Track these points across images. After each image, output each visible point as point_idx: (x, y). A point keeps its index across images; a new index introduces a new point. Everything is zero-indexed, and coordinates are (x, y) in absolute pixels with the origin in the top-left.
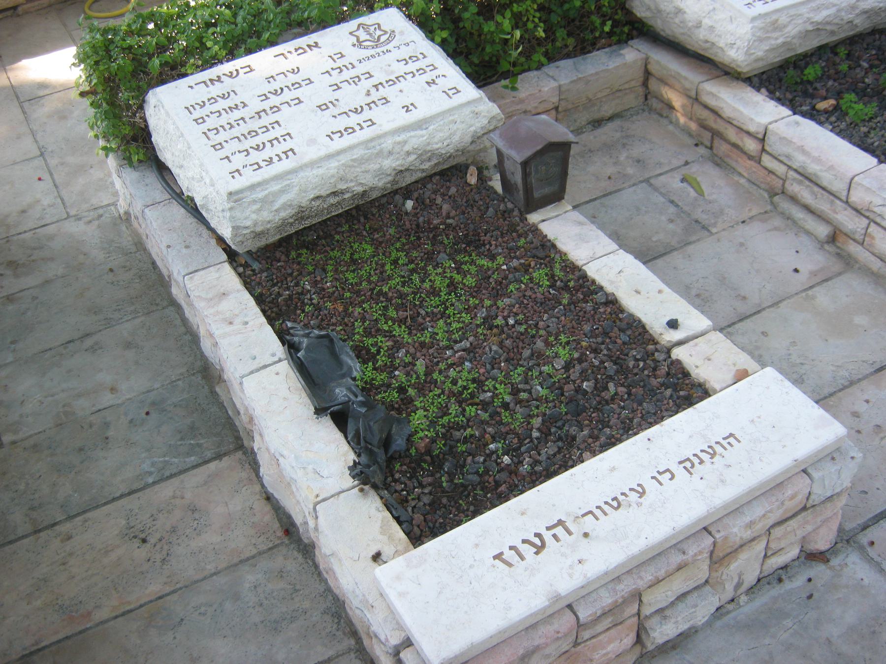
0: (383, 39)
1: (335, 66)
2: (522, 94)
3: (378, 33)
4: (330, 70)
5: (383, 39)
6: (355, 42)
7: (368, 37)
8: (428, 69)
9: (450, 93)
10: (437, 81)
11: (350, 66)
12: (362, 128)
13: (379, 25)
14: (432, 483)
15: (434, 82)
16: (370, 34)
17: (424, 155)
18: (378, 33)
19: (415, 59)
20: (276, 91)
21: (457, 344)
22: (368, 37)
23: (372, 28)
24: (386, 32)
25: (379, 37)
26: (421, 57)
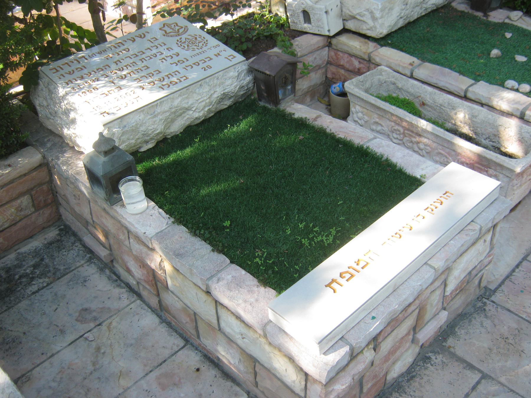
0: (181, 31)
1: (153, 45)
2: (478, 391)
3: (177, 28)
4: (150, 47)
5: (181, 31)
6: (164, 34)
7: (171, 30)
8: (206, 60)
9: (230, 58)
10: (221, 54)
11: (162, 45)
12: (181, 81)
13: (176, 24)
14: (283, 267)
15: (219, 54)
16: (173, 29)
17: (225, 96)
18: (177, 28)
19: (181, 62)
20: (70, 72)
21: (271, 181)
22: (171, 30)
23: (173, 26)
24: (182, 27)
25: (178, 30)
26: (185, 60)
